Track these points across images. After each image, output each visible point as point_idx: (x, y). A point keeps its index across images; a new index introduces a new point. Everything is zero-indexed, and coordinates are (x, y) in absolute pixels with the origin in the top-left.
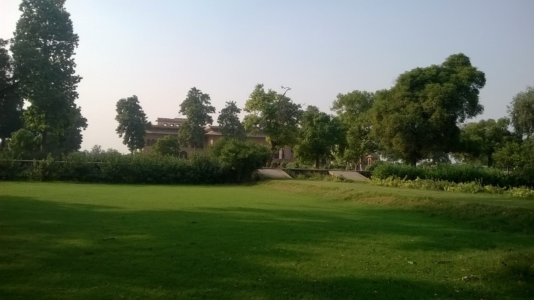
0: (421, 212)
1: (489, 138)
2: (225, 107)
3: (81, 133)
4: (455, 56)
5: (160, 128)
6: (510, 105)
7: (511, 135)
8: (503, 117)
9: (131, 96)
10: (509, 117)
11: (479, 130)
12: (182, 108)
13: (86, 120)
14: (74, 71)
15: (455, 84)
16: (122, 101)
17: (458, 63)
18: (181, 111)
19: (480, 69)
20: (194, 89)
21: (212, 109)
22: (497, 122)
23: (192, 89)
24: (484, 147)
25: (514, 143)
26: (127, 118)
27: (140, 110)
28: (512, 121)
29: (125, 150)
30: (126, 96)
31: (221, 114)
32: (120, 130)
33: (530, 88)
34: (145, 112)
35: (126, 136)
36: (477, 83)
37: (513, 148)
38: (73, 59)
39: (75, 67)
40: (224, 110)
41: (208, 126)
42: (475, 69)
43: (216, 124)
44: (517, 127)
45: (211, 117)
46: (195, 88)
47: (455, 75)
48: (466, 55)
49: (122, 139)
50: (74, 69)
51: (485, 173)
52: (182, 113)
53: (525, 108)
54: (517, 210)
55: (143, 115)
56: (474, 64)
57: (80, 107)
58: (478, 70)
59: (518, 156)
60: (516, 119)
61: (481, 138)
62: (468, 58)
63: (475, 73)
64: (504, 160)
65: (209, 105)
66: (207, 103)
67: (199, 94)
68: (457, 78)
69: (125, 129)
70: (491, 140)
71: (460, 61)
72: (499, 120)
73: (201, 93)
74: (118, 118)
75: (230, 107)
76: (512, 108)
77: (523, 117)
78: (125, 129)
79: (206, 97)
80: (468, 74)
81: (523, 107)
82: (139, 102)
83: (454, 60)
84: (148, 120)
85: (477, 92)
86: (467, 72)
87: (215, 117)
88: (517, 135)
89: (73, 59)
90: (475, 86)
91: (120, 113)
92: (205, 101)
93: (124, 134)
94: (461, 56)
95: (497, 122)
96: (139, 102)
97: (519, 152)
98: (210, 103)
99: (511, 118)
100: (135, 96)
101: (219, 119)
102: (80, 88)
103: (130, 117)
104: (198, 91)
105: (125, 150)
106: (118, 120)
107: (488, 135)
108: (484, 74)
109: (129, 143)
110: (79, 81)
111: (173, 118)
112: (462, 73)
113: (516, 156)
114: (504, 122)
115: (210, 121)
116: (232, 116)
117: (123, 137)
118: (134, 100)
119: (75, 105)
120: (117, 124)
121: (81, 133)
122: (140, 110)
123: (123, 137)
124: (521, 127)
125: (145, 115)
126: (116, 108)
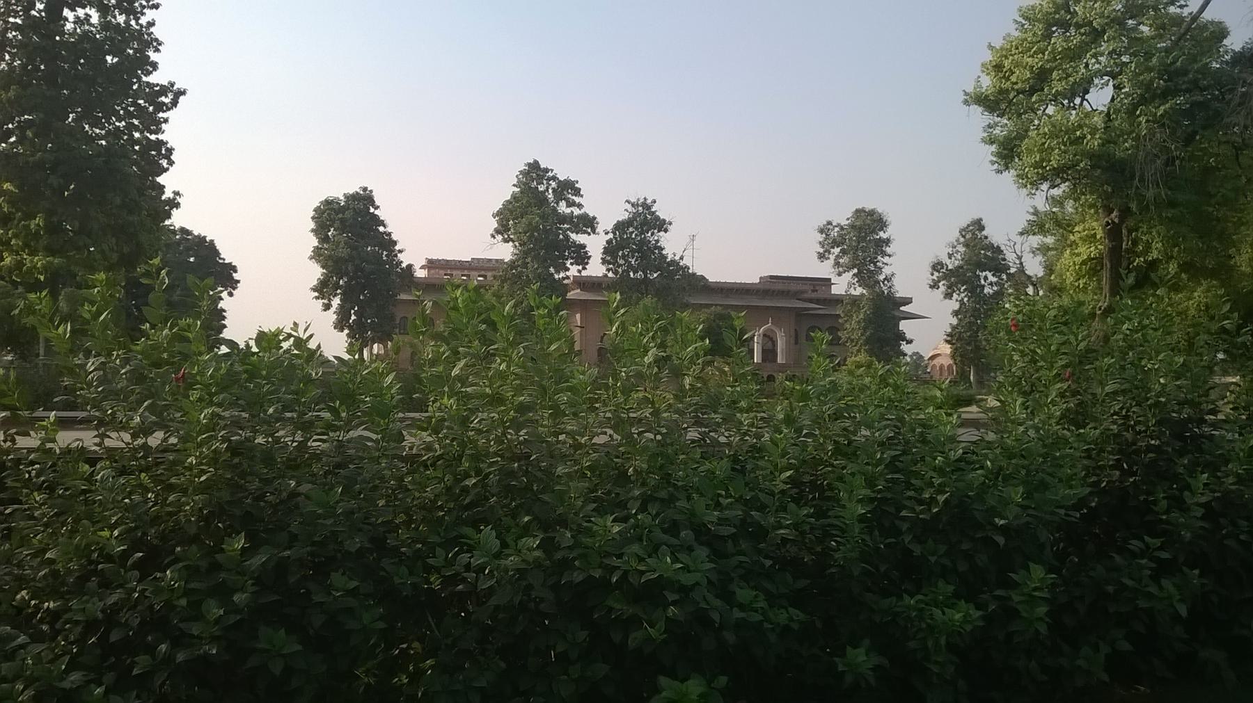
2: (625, 216)
3: (221, 305)
5: (434, 285)
9: (353, 188)
12: (500, 222)
13: (234, 269)
14: (155, 66)
16: (328, 202)
18: (498, 231)
20: (534, 166)
21: (588, 224)
23: (529, 165)
26: (343, 252)
27: (381, 229)
29: (333, 344)
30: (340, 189)
31: (611, 236)
32: (323, 289)
34: (394, 237)
35: (341, 306)
38: (151, 24)
39: (157, 50)
40: (620, 227)
41: (573, 270)
43: (596, 269)
45: (583, 246)
46: (536, 162)
48: (869, 206)
49: (331, 316)
50: (153, 56)
52: (500, 237)
55: (388, 243)
57: (177, 193)
65: (577, 212)
66: (571, 204)
67: (549, 179)
69: (337, 286)
73: (554, 178)
74: (317, 255)
75: (637, 215)
78: (337, 286)
79: (568, 188)
82: (377, 208)
84: (405, 259)
87: (595, 244)
89: (151, 24)
91: (324, 239)
92: (567, 200)
93: (336, 302)
96: (377, 208)
98: (580, 206)
100: (365, 189)
101: (606, 251)
102: (177, 129)
103: (354, 248)
104: (547, 170)
105: (333, 344)
106: (318, 261)
109: (350, 327)
110: (175, 103)
111: (467, 258)
115: (582, 257)
116: (644, 242)
117: (333, 309)
118: (362, 202)
119: (161, 188)
120: (316, 272)
121: (221, 305)
122: (381, 229)
123: (333, 309)
125: (395, 243)
126: (312, 225)
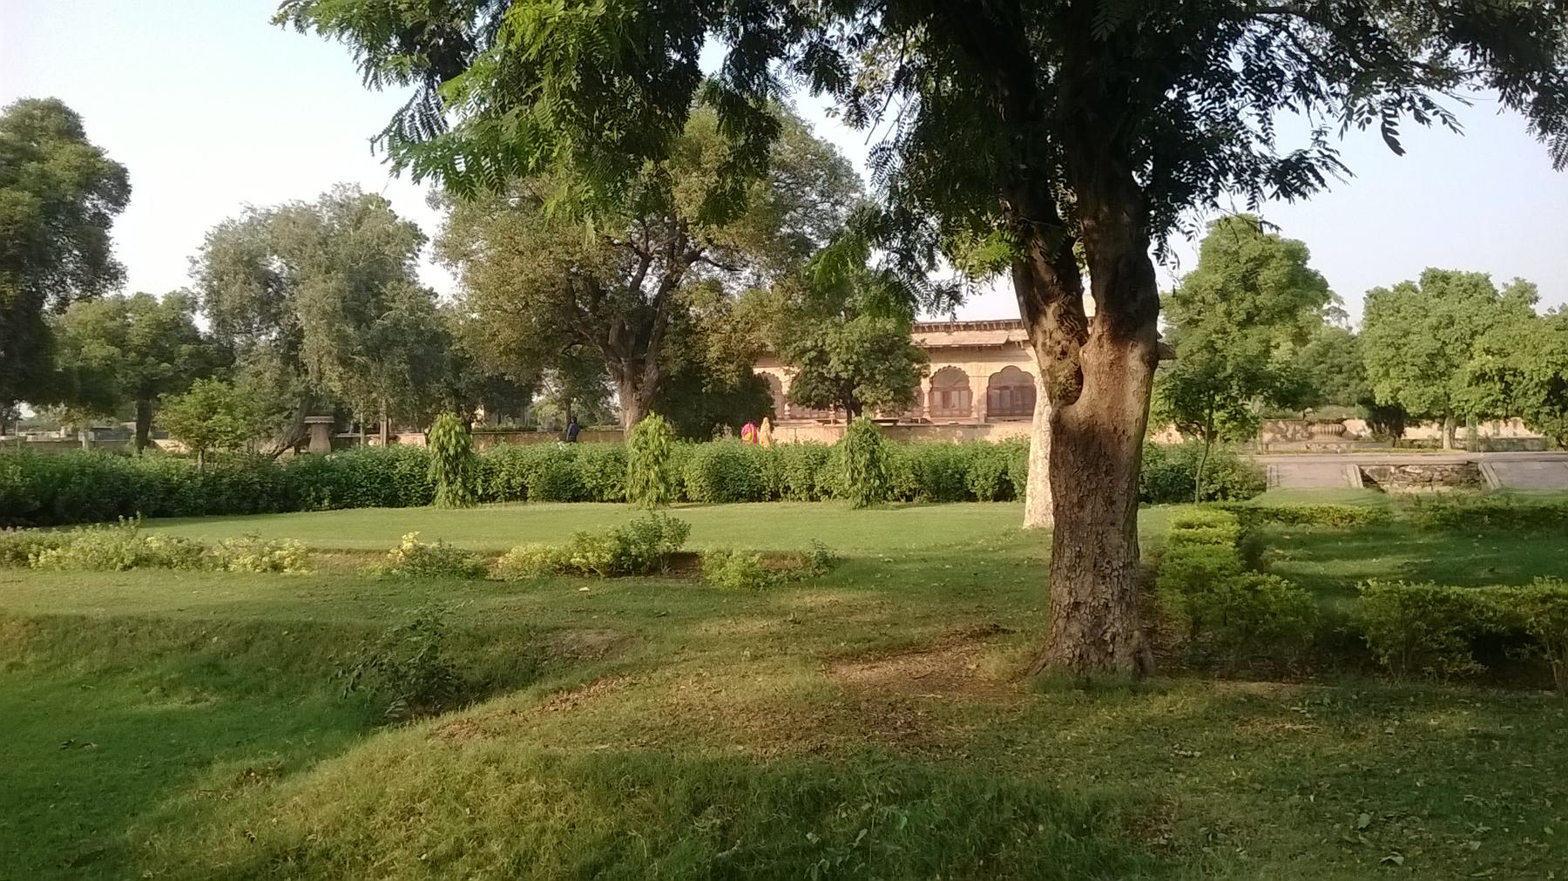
0: (106, 672)
1: (137, 349)
4: (34, 103)
6: (198, 255)
7: (201, 342)
8: (179, 290)
10: (197, 290)
11: (109, 324)
15: (38, 194)
17: (42, 129)
19: (115, 153)
22: (160, 301)
24: (125, 376)
25: (216, 384)
28: (207, 302)
33: (253, 210)
36: (105, 195)
37: (213, 398)
42: (97, 153)
44: (220, 320)
47: (34, 164)
48: (71, 104)
51: (138, 470)
53: (240, 267)
54: (249, 628)
56: (95, 135)
58: (106, 157)
59: (229, 419)
60: (214, 297)
61: (115, 350)
62: (76, 117)
63: (99, 165)
64: (190, 431)
68: (43, 176)
70: (146, 355)
71: (53, 122)
72: (168, 297)
76: (203, 266)
77: (233, 294)
80: (77, 168)
81: (235, 263)
83: (32, 117)
85: (105, 222)
86: (77, 162)
88: (218, 341)
90: (100, 203)
94: (55, 108)
95: (160, 301)
97: (230, 409)
99: (203, 292)
107: (137, 341)
108: (125, 171)
112: (61, 161)
113: (221, 419)
114: (183, 302)
124: (229, 318)
